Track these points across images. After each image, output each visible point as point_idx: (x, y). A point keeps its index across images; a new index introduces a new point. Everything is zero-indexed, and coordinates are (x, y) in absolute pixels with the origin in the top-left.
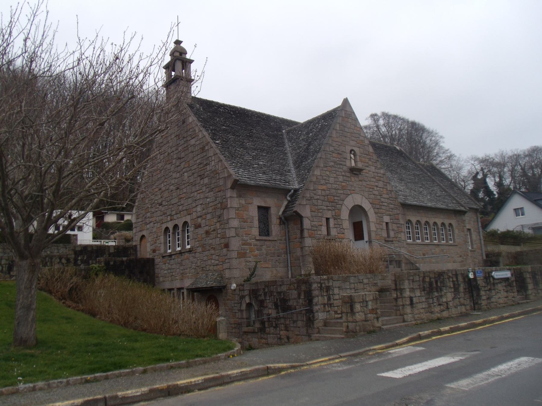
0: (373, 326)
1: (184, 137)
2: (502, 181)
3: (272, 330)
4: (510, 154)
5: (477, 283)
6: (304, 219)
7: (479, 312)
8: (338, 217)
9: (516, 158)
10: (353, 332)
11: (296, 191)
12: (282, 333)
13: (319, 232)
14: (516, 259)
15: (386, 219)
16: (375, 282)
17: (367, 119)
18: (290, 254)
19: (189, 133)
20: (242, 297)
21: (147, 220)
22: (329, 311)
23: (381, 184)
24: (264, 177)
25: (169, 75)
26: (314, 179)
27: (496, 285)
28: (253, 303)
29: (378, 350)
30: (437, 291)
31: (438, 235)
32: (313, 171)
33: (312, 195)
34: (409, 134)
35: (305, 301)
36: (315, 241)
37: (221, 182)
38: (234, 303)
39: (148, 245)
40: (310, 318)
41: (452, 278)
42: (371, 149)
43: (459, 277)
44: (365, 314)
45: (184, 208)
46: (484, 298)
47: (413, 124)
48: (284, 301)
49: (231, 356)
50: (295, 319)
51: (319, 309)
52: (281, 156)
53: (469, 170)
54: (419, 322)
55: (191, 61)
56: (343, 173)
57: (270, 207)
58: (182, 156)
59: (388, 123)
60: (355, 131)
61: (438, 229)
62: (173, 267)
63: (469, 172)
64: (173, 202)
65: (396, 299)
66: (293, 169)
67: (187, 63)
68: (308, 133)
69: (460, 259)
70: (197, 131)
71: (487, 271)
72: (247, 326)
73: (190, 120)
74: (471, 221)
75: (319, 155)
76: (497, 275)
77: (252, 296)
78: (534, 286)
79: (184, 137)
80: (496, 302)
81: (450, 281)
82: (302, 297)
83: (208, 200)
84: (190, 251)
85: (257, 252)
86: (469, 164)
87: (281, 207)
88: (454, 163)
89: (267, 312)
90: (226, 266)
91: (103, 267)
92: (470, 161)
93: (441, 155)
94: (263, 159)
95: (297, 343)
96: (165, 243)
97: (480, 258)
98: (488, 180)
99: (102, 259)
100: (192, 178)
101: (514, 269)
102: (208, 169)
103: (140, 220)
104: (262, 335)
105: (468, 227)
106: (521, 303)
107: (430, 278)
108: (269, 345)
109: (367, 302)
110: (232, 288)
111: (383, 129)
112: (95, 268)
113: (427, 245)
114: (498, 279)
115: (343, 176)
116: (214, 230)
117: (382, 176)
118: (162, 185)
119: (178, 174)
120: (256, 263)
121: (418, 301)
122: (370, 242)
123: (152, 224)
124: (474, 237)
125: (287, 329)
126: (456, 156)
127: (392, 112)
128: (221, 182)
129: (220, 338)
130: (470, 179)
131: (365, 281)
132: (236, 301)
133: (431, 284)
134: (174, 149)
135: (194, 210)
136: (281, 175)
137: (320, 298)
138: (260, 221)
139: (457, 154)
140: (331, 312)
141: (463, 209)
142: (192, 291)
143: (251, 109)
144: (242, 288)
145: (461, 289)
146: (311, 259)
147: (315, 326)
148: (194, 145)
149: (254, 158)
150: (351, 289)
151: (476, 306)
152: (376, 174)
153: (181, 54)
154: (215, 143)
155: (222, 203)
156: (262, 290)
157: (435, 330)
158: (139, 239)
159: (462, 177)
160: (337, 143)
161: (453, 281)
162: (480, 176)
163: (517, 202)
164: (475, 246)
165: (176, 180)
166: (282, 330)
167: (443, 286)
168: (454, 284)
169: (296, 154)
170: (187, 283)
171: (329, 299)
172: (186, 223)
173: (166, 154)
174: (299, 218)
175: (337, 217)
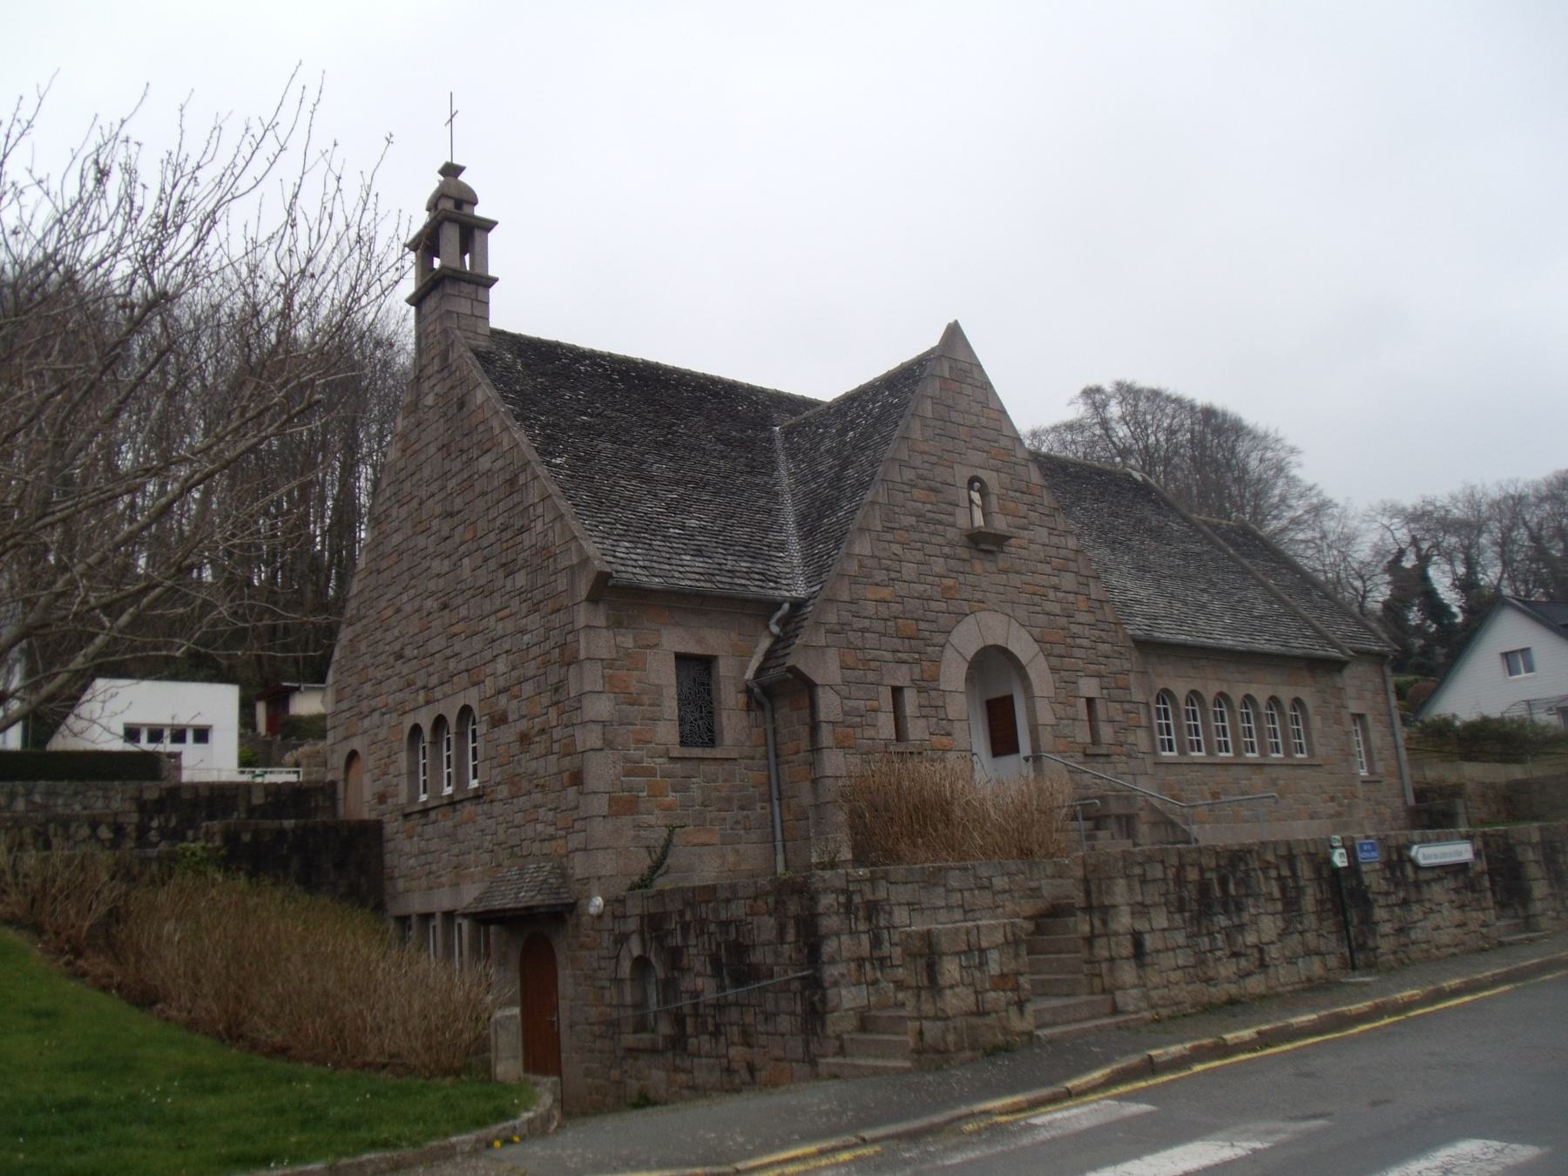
0: (1006, 1031)
1: (462, 451)
2: (1475, 573)
3: (705, 1043)
4: (1495, 494)
5: (1360, 882)
6: (820, 691)
7: (1368, 975)
8: (932, 685)
9: (1513, 507)
10: (938, 1052)
11: (798, 605)
12: (733, 1052)
13: (870, 733)
14: (1513, 802)
15: (1089, 687)
16: (1033, 884)
17: (1072, 403)
18: (780, 799)
19: (476, 438)
20: (622, 939)
21: (365, 706)
22: (875, 982)
23: (1068, 581)
24: (699, 564)
25: (424, 266)
26: (853, 567)
27: (1425, 888)
28: (653, 959)
29: (1001, 1114)
30: (1226, 912)
31: (1286, 738)
32: (851, 543)
33: (847, 617)
34: (1197, 442)
35: (800, 950)
36: (855, 760)
37: (562, 583)
38: (600, 958)
39: (367, 779)
40: (812, 1004)
41: (1277, 868)
42: (1035, 476)
43: (1299, 864)
44: (976, 992)
45: (462, 666)
46: (1386, 928)
47: (1209, 414)
48: (739, 949)
49: (497, 1144)
50: (770, 1007)
51: (843, 975)
52: (761, 502)
53: (1375, 545)
54: (1164, 1012)
55: (488, 225)
56: (946, 550)
57: (715, 657)
58: (456, 508)
59: (1135, 412)
60: (983, 421)
61: (1258, 716)
62: (434, 845)
63: (1378, 552)
64: (434, 646)
65: (1090, 940)
66: (794, 539)
67: (473, 231)
68: (842, 432)
69: (1332, 807)
70: (497, 431)
71: (1393, 842)
72: (635, 1032)
73: (479, 397)
74: (1361, 690)
75: (869, 496)
76: (1425, 857)
77: (647, 936)
78: (1551, 885)
79: (462, 451)
80: (1428, 942)
81: (1267, 878)
82: (791, 937)
83: (526, 638)
84: (478, 796)
85: (671, 797)
86: (1375, 525)
87: (751, 655)
88: (1329, 525)
89: (691, 987)
90: (575, 841)
91: (218, 849)
92: (1379, 518)
93: (1293, 502)
94: (699, 511)
95: (775, 1085)
96: (413, 774)
97: (1398, 802)
98: (1432, 572)
99: (216, 825)
100: (481, 572)
101: (1484, 834)
102: (527, 544)
103: (345, 705)
104: (678, 1061)
105: (1354, 707)
106: (1511, 944)
107: (1202, 871)
108: (697, 1091)
109: (982, 951)
110: (592, 910)
111: (1122, 431)
112: (193, 854)
113: (1225, 765)
114: (1432, 868)
115: (947, 557)
116: (543, 731)
117: (1071, 556)
118: (405, 597)
119: (446, 562)
120: (672, 830)
121: (1160, 946)
122: (1036, 758)
123: (376, 715)
124: (1376, 738)
125: (747, 1039)
126: (1336, 506)
127: (1146, 380)
128: (562, 583)
129: (500, 1077)
130: (1378, 570)
131: (1000, 882)
132: (605, 953)
133: (1204, 888)
134: (435, 487)
135: (489, 670)
136: (754, 557)
137: (844, 938)
138: (683, 701)
139: (1339, 498)
140: (883, 984)
141: (1334, 653)
142: (483, 919)
143: (694, 369)
144: (619, 909)
145: (1308, 903)
146: (841, 817)
147: (830, 1030)
148: (488, 474)
149: (672, 508)
150: (949, 908)
151: (1358, 954)
152: (1053, 552)
153: (459, 204)
154: (548, 464)
155: (562, 646)
156: (675, 917)
157: (1205, 1041)
158: (342, 763)
159: (1355, 565)
160: (926, 457)
161: (1280, 878)
162: (1409, 562)
163: (1509, 630)
164: (1380, 767)
165: (442, 581)
166: (733, 1044)
167: (1247, 896)
168: (1283, 889)
169: (805, 494)
170: (469, 896)
171: (876, 942)
172: (466, 712)
173: (415, 503)
174: (804, 687)
175: (927, 684)
